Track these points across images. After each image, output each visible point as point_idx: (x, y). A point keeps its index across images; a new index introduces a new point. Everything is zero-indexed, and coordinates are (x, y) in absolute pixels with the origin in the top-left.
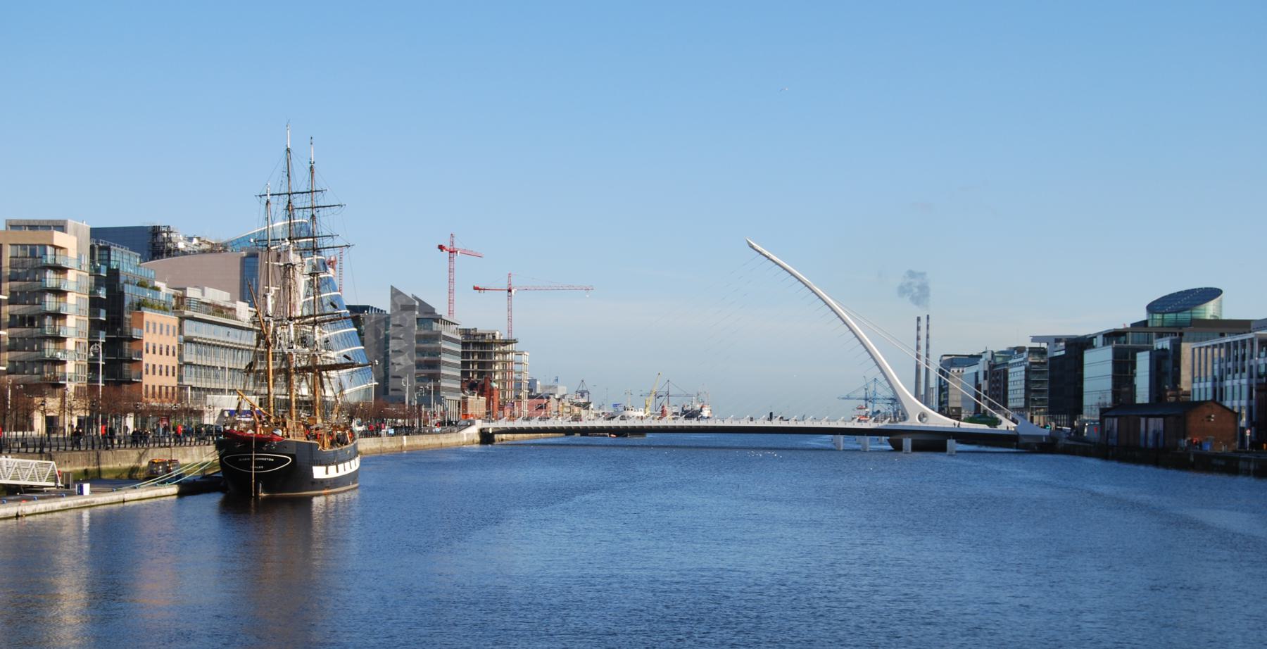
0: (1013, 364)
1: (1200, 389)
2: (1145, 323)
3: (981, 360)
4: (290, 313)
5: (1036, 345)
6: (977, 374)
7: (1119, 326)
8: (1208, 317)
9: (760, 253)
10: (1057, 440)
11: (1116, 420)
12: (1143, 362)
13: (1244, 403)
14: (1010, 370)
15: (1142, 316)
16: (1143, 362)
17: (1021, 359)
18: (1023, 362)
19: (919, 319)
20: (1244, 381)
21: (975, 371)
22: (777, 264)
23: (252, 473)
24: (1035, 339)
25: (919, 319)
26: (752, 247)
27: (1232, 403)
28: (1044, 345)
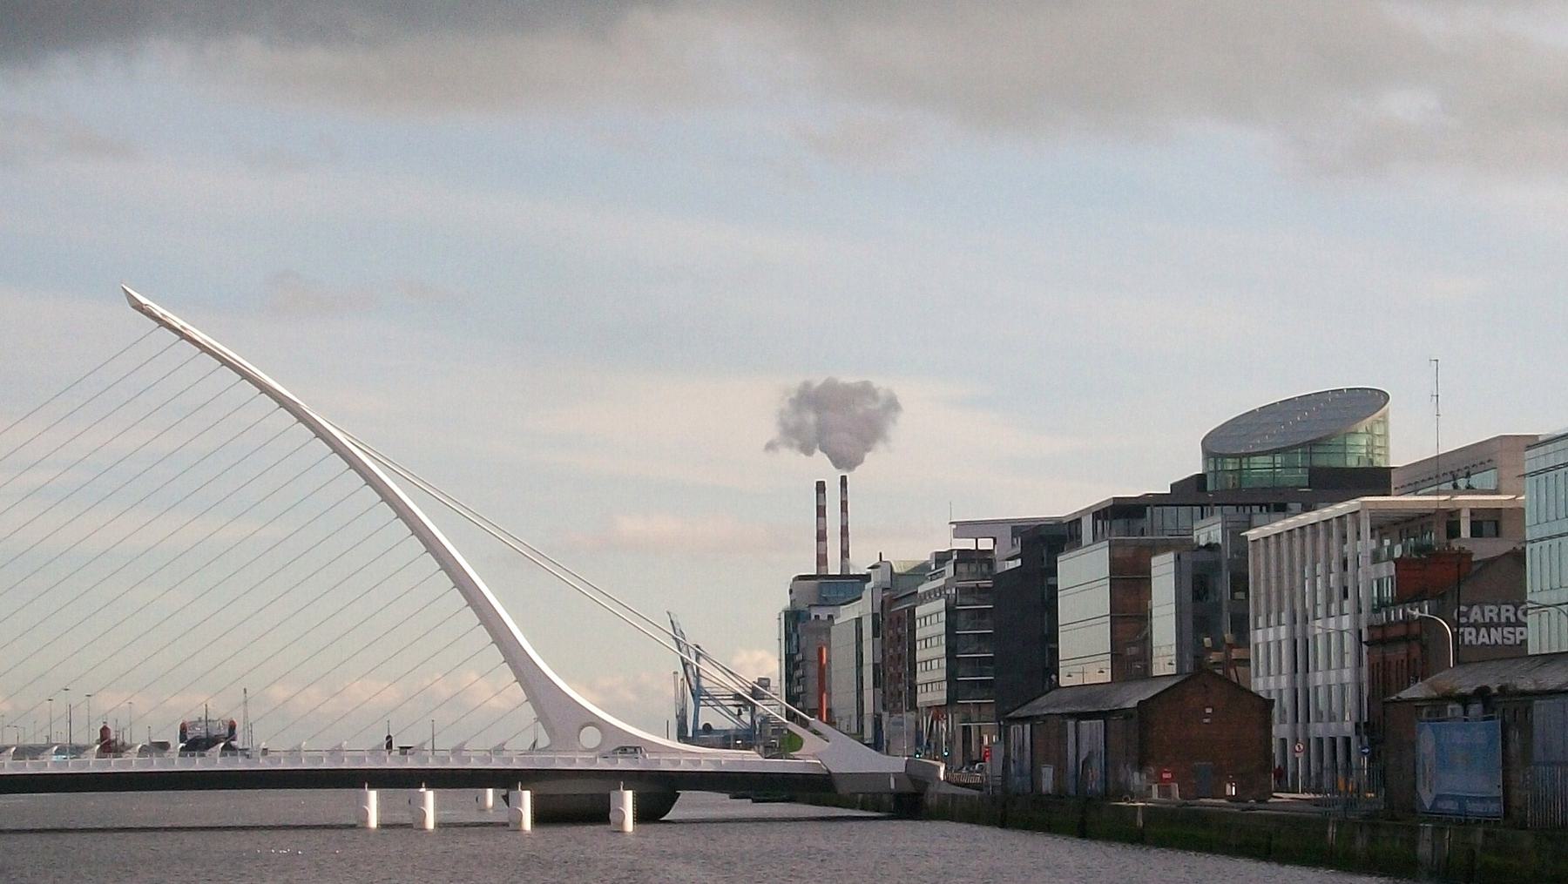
0: (928, 593)
1: (1268, 644)
2: (1200, 480)
3: (869, 586)
4: (845, 554)
5: (968, 544)
6: (859, 620)
7: (1133, 491)
8: (1352, 462)
9: (161, 322)
10: (927, 784)
11: (1028, 726)
12: (1163, 573)
13: (1284, 681)
14: (919, 611)
15: (1195, 466)
16: (1163, 573)
17: (940, 582)
18: (945, 587)
19: (821, 487)
20: (1346, 622)
21: (1529, 625)
22: (204, 349)
23: (1143, 807)
24: (962, 528)
25: (821, 487)
26: (139, 307)
27: (1266, 683)
28: (986, 544)
